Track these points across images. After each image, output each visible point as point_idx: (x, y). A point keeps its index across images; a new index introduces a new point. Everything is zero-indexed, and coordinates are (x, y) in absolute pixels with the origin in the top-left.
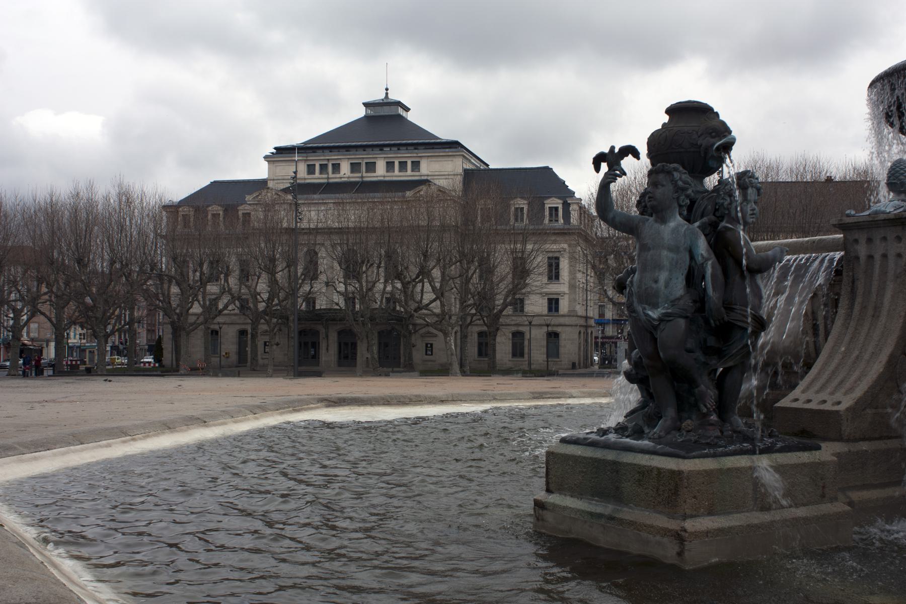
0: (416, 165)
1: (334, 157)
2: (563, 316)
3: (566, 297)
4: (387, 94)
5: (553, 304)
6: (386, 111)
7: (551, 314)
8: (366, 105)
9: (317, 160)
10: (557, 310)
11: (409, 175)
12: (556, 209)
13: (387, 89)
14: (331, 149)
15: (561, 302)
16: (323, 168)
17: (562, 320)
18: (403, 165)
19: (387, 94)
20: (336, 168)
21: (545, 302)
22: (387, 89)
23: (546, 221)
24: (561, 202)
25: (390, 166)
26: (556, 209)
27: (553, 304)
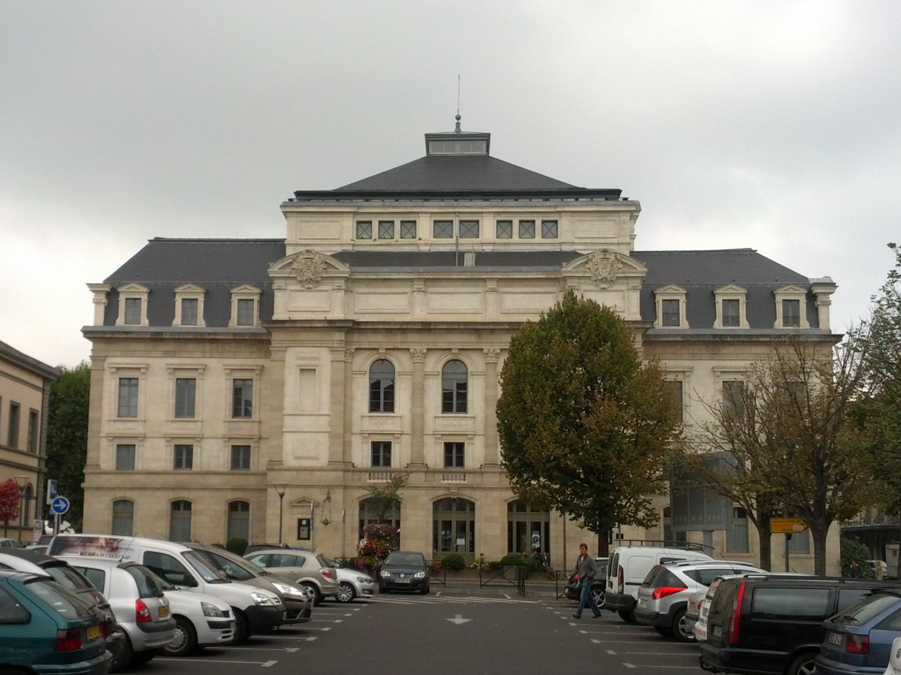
0: (551, 226)
1: (406, 206)
2: (473, 472)
3: (406, 440)
4: (458, 124)
5: (183, 455)
6: (457, 150)
7: (377, 468)
8: (430, 139)
9: (375, 209)
10: (460, 462)
11: (538, 243)
12: (137, 300)
13: (458, 118)
14: (397, 195)
15: (468, 450)
16: (386, 225)
17: (469, 480)
18: (386, 225)
19: (458, 124)
20: (410, 225)
21: (440, 450)
22: (458, 118)
23: (177, 321)
24: (257, 291)
25: (504, 225)
26: (137, 300)
27: (183, 455)
